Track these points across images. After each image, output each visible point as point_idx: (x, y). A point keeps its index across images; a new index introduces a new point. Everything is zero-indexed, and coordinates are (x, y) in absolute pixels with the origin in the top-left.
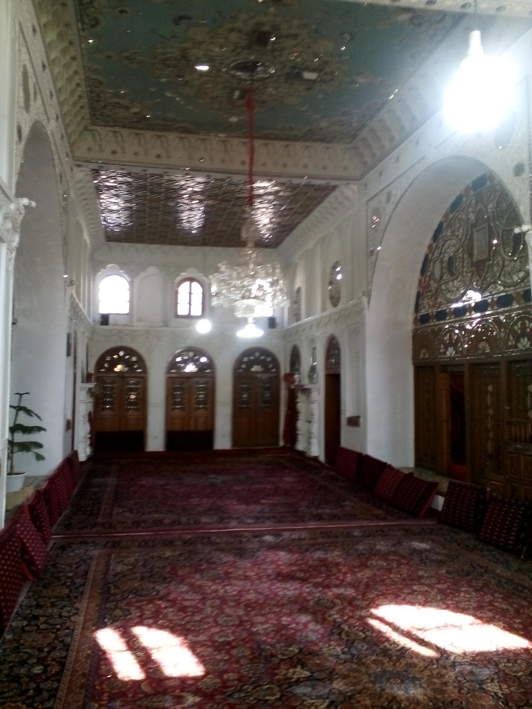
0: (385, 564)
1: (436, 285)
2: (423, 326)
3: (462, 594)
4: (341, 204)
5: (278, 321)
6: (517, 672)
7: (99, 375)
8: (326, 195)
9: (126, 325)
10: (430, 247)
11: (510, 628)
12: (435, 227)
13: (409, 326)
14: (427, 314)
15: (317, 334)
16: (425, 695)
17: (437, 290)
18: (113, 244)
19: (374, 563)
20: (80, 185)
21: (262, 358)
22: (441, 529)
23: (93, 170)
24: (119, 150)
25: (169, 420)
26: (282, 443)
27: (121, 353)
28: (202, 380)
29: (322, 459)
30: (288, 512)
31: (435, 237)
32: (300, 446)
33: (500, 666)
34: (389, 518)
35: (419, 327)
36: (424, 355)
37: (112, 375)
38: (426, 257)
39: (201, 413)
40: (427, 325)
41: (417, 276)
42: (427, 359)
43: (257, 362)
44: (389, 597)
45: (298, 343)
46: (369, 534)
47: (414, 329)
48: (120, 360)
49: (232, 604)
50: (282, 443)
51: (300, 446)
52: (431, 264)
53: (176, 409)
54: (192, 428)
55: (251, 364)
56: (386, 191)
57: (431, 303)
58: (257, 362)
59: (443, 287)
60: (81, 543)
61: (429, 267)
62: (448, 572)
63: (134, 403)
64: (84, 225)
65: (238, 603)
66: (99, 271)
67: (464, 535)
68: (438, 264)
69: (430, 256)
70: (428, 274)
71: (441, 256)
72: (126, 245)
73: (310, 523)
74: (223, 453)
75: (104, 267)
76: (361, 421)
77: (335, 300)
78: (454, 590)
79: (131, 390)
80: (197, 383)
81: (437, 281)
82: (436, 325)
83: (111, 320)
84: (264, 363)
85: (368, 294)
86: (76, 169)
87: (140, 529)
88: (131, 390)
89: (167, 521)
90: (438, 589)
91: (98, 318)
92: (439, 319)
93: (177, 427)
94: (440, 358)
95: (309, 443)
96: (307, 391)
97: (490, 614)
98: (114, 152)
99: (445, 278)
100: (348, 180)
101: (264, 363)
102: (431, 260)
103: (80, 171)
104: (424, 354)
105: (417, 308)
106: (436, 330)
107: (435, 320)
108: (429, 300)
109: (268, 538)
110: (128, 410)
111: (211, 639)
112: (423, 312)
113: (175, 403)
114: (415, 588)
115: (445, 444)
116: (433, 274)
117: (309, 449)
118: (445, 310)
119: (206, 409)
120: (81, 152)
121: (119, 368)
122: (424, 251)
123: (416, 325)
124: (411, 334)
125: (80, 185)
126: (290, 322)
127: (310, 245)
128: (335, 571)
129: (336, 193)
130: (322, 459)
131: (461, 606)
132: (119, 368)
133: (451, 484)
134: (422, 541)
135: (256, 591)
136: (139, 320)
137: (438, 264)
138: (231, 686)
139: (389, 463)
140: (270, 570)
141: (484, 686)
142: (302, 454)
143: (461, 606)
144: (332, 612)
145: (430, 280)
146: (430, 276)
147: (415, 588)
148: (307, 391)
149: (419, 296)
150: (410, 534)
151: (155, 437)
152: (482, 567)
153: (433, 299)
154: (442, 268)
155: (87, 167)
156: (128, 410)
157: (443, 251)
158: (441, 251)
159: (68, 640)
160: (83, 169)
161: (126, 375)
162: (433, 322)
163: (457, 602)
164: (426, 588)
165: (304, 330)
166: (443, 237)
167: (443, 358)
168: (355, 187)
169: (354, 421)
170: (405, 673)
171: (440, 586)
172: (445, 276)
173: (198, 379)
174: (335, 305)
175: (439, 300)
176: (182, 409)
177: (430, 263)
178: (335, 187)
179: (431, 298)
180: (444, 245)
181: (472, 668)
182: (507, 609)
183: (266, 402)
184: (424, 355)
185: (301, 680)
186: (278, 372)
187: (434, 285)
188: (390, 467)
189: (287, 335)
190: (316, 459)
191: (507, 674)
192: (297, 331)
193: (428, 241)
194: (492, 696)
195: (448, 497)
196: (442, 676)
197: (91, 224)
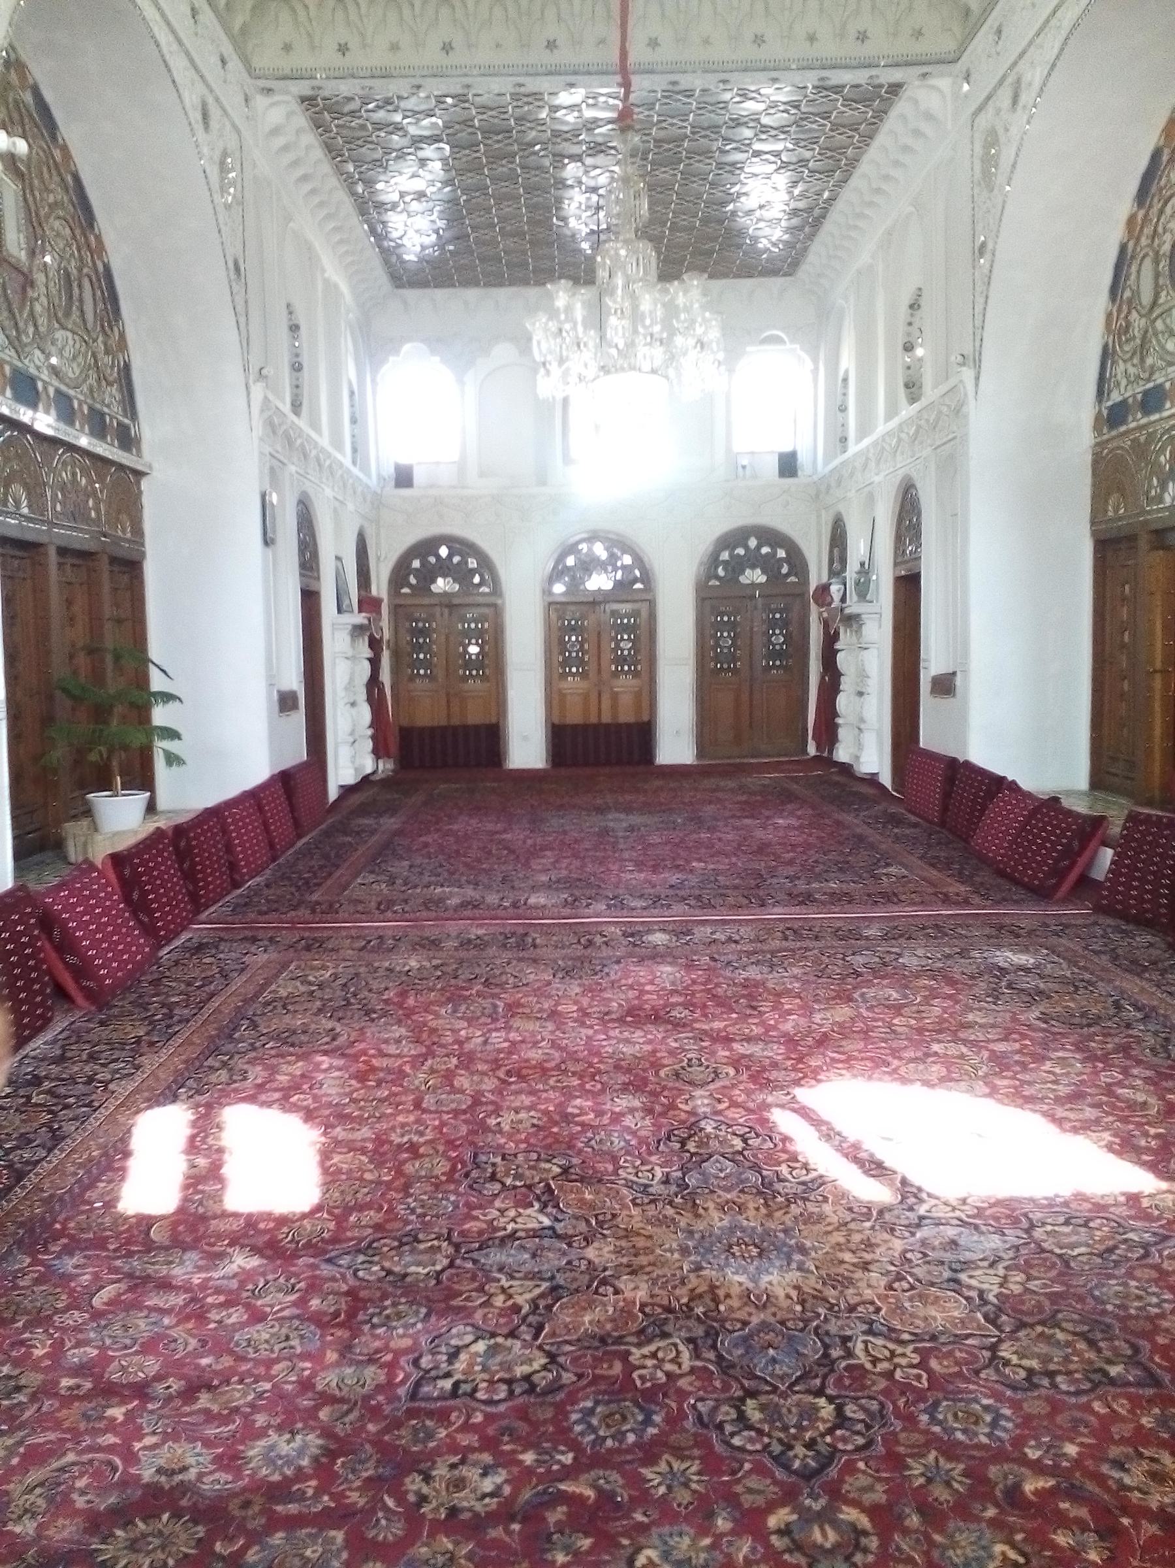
0: (895, 995)
1: (1143, 320)
2: (1114, 433)
3: (1048, 1066)
4: (917, 133)
5: (803, 458)
6: (1072, 1246)
7: (398, 601)
8: (881, 114)
9: (454, 487)
10: (1131, 220)
11: (1126, 1148)
12: (1143, 163)
13: (1083, 439)
14: (1125, 401)
15: (877, 479)
16: (797, 1288)
17: (1146, 332)
18: (411, 294)
19: (871, 993)
20: (280, 141)
21: (765, 550)
22: (1096, 923)
23: (303, 99)
24: (354, 43)
25: (553, 698)
26: (812, 750)
27: (472, 563)
28: (624, 608)
29: (886, 780)
30: (736, 887)
31: (1142, 195)
32: (842, 754)
33: (1038, 1233)
34: (976, 900)
35: (1105, 437)
36: (1116, 510)
37: (426, 601)
38: (1123, 248)
39: (625, 684)
40: (1123, 429)
41: (1102, 301)
42: (1120, 519)
43: (754, 560)
44: (858, 1065)
45: (841, 508)
46: (896, 934)
47: (1097, 444)
48: (444, 569)
49: (481, 1067)
50: (812, 750)
51: (842, 754)
52: (1134, 269)
53: (571, 674)
54: (606, 718)
55: (737, 566)
56: (1010, 80)
57: (1132, 370)
58: (754, 560)
59: (1159, 325)
60: (245, 939)
61: (1127, 277)
62: (1045, 1018)
63: (479, 663)
64: (318, 245)
65: (304, 1032)
66: (383, 362)
67: (1143, 938)
68: (1148, 264)
69: (1131, 245)
70: (1127, 294)
71: (1157, 241)
72: (440, 294)
73: (776, 910)
74: (676, 772)
75: (397, 352)
76: (959, 680)
77: (913, 388)
78: (1031, 1055)
79: (467, 634)
80: (614, 613)
81: (1143, 312)
82: (1140, 428)
83: (419, 477)
84: (768, 565)
85: (974, 360)
86: (260, 101)
87: (389, 914)
88: (467, 634)
89: (453, 902)
90: (993, 1052)
91: (389, 471)
92: (1147, 411)
93: (574, 717)
94: (1149, 512)
95: (860, 746)
96: (852, 620)
97: (1090, 1113)
98: (343, 49)
99: (1161, 301)
100: (927, 64)
101: (768, 565)
102: (1133, 257)
103: (273, 105)
104: (1115, 508)
105: (1101, 392)
106: (1142, 439)
107: (1139, 415)
108: (1129, 365)
109: (659, 938)
110: (465, 679)
111: (380, 1140)
112: (1116, 397)
113: (566, 663)
114: (936, 1047)
115: (1158, 731)
116: (1136, 293)
117: (857, 758)
118: (1161, 386)
119: (636, 674)
120: (268, 57)
121: (441, 584)
122: (1116, 234)
123: (1100, 434)
124: (1089, 458)
125: (280, 141)
126: (828, 459)
127: (864, 258)
128: (765, 1006)
129: (901, 107)
130: (886, 780)
131: (1028, 1091)
132: (441, 584)
133: (1133, 818)
134: (1025, 950)
135: (554, 1044)
136: (482, 474)
137: (1148, 263)
138: (352, 1239)
139: (1010, 778)
140: (617, 1001)
141: (963, 1277)
142: (846, 769)
143: (1028, 1091)
144: (698, 1093)
145: (1129, 312)
146: (1130, 301)
147: (936, 1047)
148: (852, 620)
149: (1107, 355)
150: (1004, 933)
151: (525, 738)
152: (1138, 1009)
153: (1135, 361)
154: (1157, 275)
155: (287, 93)
156: (465, 679)
157: (1160, 229)
158: (1155, 231)
159: (69, 1127)
160: (277, 98)
161: (456, 601)
162: (1137, 420)
163: (1023, 1082)
164: (964, 1050)
165: (852, 475)
166: (1161, 189)
167: (1159, 510)
168: (944, 83)
169: (945, 686)
170: (781, 1235)
171: (1001, 1047)
172: (1164, 294)
173: (615, 606)
174: (913, 400)
175: (1149, 361)
176: (584, 675)
177: (1129, 266)
178: (895, 89)
179: (1131, 358)
180: (1161, 212)
181: (960, 1234)
182: (1145, 1103)
183: (774, 654)
184: (1116, 510)
185: (519, 1234)
186: (805, 581)
187: (1138, 323)
188: (1013, 787)
189: (820, 491)
190: (872, 780)
191: (1043, 1251)
192: (838, 478)
193: (1125, 206)
194: (967, 1299)
195: (1122, 847)
196: (869, 1245)
197: (341, 242)
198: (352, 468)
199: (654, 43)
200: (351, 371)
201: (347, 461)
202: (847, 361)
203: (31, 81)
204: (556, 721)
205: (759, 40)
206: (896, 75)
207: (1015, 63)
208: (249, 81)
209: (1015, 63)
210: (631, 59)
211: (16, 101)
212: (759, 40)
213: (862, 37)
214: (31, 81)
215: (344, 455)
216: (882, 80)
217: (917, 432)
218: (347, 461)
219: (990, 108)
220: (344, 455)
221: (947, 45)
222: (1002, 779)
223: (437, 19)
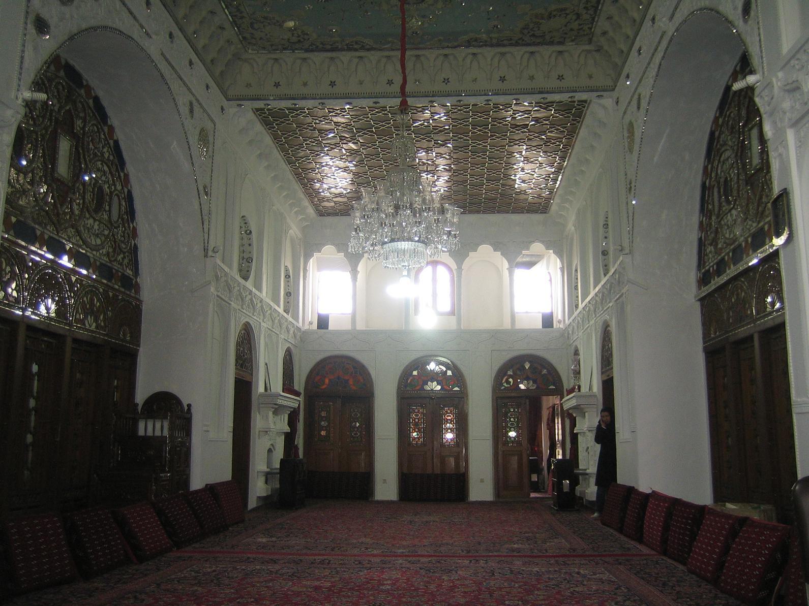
54: (438, 471)
83: (332, 326)
198: (285, 314)
199: (390, 82)
200: (287, 261)
201: (281, 310)
202: (576, 261)
203: (115, 138)
204: (405, 471)
205: (503, 79)
206: (584, 96)
207: (636, 89)
208: (226, 102)
209: (636, 89)
210: (408, 89)
211: (486, 588)
212: (560, 78)
213: (446, 81)
214: (115, 138)
215: (279, 306)
216: (575, 99)
217: (611, 287)
218: (281, 310)
219: (629, 112)
220: (279, 306)
221: (609, 83)
222: (676, 500)
223: (528, 66)
